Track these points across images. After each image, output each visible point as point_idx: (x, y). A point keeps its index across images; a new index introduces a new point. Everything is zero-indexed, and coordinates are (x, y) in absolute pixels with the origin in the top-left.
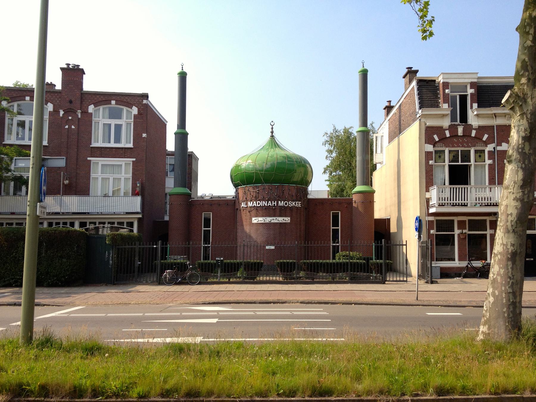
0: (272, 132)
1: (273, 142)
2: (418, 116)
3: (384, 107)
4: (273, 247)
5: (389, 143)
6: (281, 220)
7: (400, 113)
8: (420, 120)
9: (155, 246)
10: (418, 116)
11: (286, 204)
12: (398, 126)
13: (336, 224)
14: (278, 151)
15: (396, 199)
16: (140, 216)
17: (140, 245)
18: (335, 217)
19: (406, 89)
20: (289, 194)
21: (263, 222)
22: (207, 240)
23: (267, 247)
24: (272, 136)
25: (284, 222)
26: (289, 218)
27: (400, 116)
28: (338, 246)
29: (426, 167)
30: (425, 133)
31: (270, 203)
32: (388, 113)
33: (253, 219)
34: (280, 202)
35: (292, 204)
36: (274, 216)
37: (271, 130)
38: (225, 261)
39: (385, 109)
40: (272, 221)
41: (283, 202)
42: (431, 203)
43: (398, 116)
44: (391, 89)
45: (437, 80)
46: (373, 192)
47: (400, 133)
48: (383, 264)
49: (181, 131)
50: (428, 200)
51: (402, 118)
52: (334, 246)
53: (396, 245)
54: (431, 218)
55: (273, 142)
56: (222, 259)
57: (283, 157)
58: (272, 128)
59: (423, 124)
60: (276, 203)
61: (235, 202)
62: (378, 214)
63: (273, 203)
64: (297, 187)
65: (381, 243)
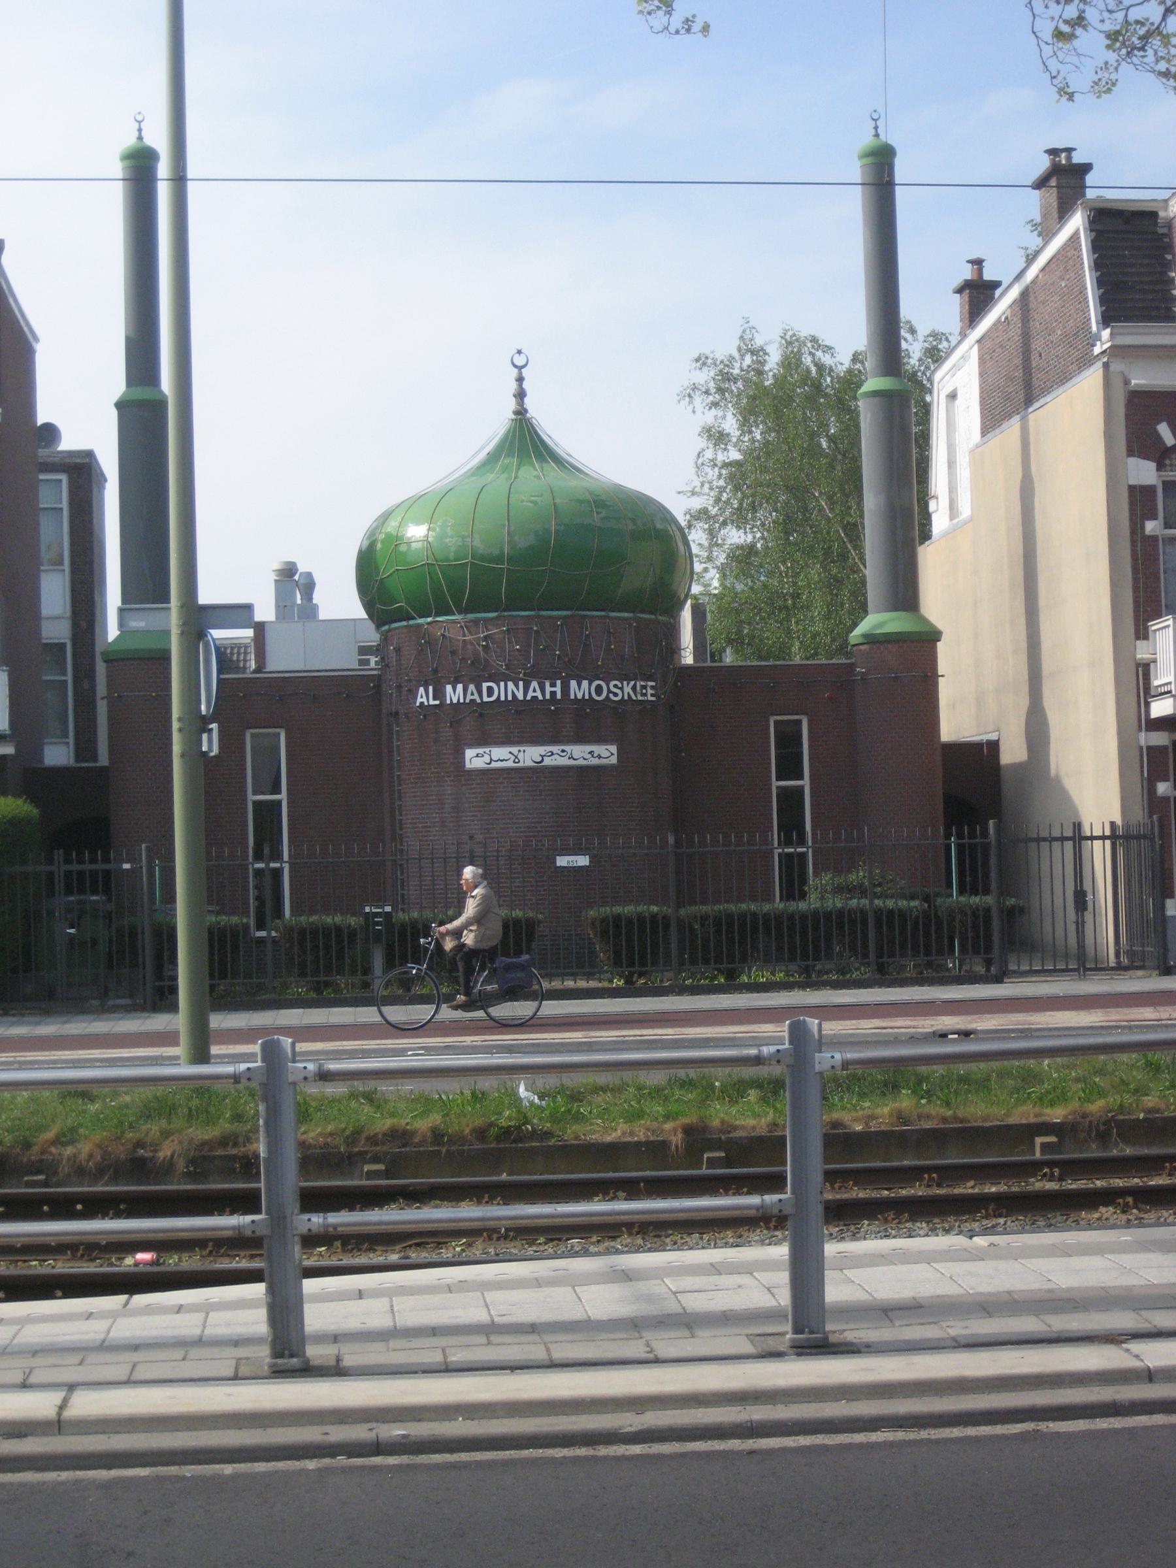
0: (521, 395)
1: (524, 441)
2: (1097, 350)
3: (958, 281)
4: (583, 861)
6: (580, 754)
8: (1106, 366)
9: (127, 866)
10: (1097, 350)
11: (599, 690)
12: (1019, 374)
13: (790, 766)
14: (552, 473)
18: (789, 739)
20: (608, 650)
21: (510, 764)
23: (562, 861)
24: (521, 412)
26: (613, 749)
27: (1026, 339)
28: (803, 856)
29: (1133, 542)
30: (1127, 416)
31: (534, 691)
33: (470, 753)
34: (573, 683)
35: (624, 690)
37: (514, 386)
38: (402, 916)
39: (959, 291)
40: (548, 761)
41: (585, 683)
42: (1156, 683)
43: (1015, 332)
44: (981, 224)
45: (1162, 214)
47: (1029, 400)
48: (995, 913)
49: (142, 393)
50: (1145, 670)
53: (1028, 840)
54: (1160, 739)
55: (524, 441)
56: (388, 909)
57: (580, 502)
58: (520, 380)
59: (1118, 383)
60: (558, 689)
61: (378, 688)
62: (955, 724)
63: (548, 689)
64: (638, 620)
65: (985, 833)
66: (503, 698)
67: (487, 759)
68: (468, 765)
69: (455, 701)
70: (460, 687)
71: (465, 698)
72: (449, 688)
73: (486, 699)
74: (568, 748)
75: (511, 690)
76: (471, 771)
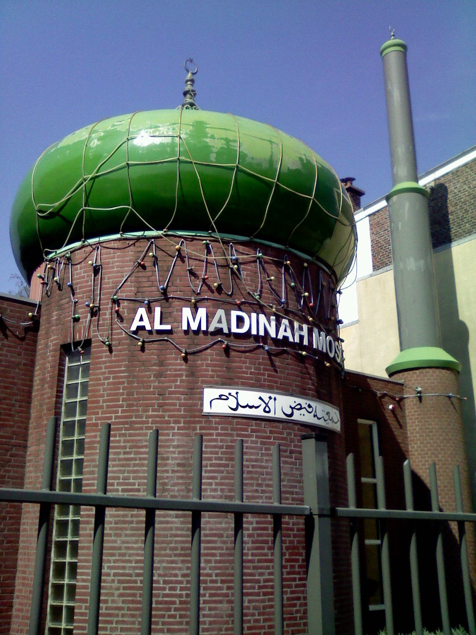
21: (259, 412)
33: (210, 393)
40: (297, 416)
66: (254, 332)
67: (232, 402)
68: (207, 409)
69: (194, 327)
70: (202, 312)
71: (277, 334)
72: (187, 312)
73: (234, 329)
74: (313, 404)
75: (257, 323)
76: (209, 416)
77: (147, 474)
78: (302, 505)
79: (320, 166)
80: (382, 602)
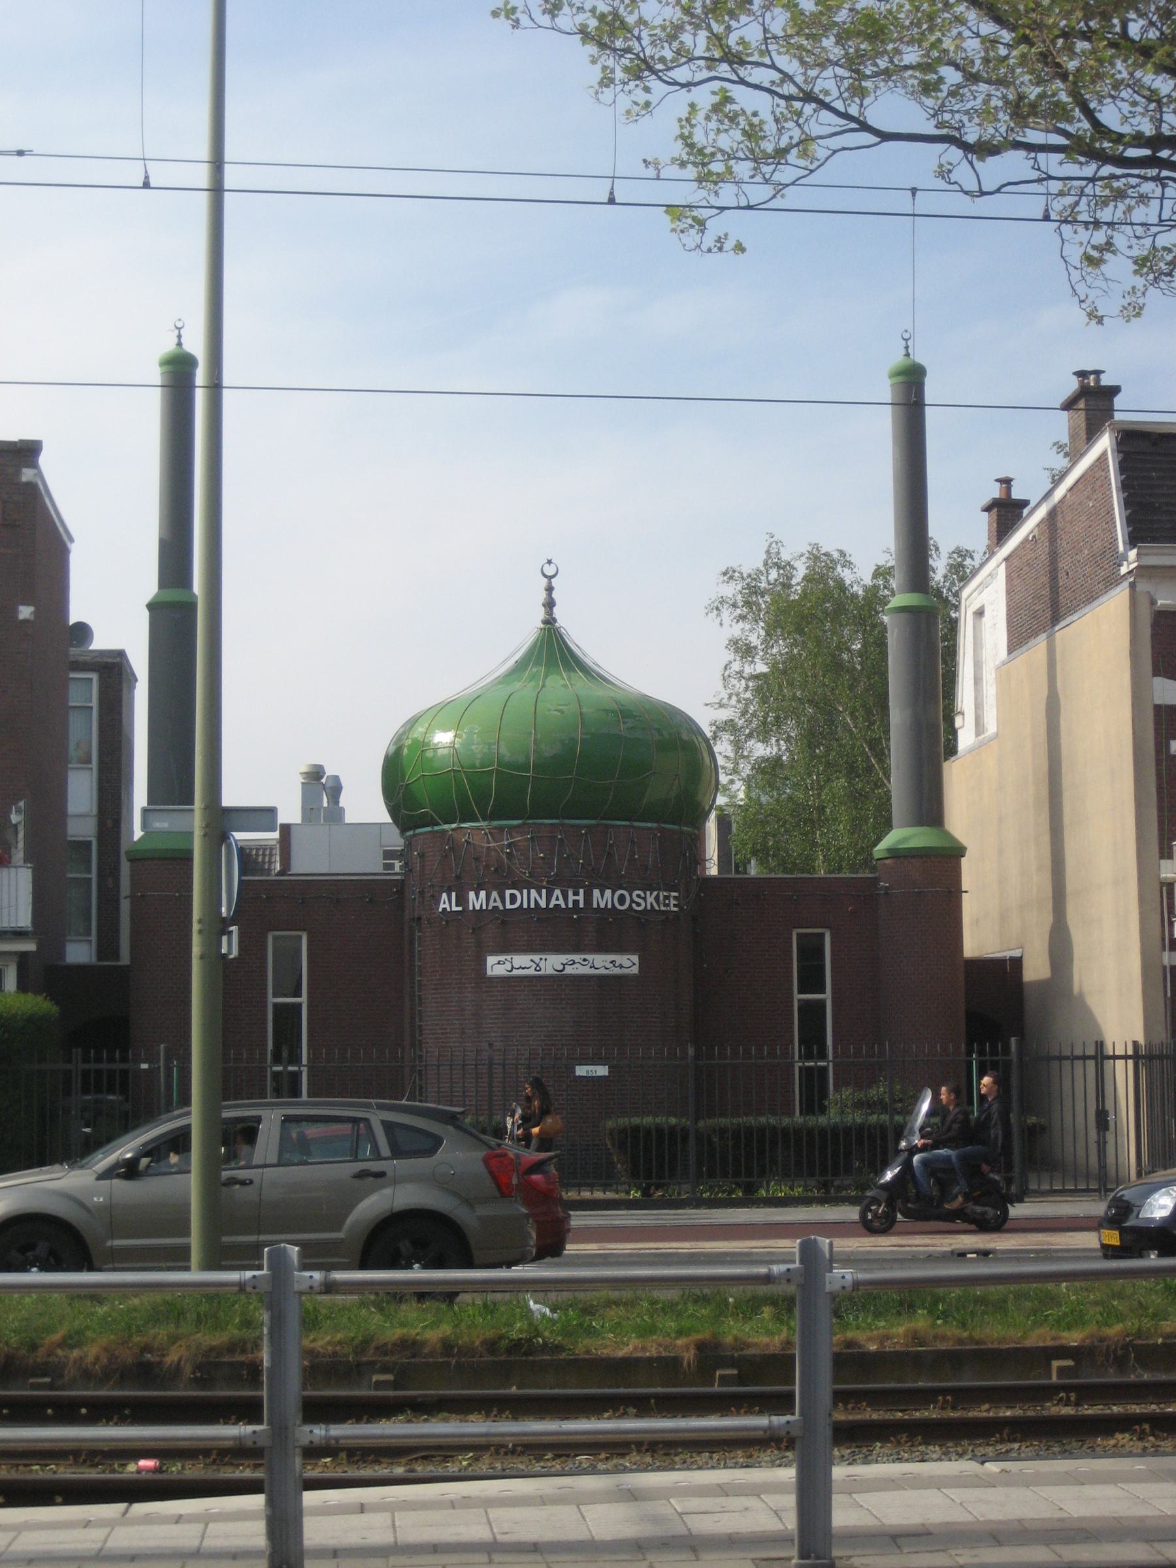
0: (550, 604)
1: (552, 650)
2: (1124, 570)
3: (986, 500)
4: (602, 1071)
5: (1011, 650)
6: (601, 963)
7: (1053, 540)
8: (1132, 586)
9: (144, 1066)
10: (1124, 570)
11: (622, 899)
12: (1046, 592)
15: (1042, 882)
16: (30, 946)
17: (86, 1060)
18: (811, 952)
19: (1075, 455)
21: (531, 972)
22: (813, 1040)
23: (581, 1071)
24: (550, 621)
25: (617, 971)
26: (635, 959)
28: (825, 1069)
29: (1158, 762)
31: (557, 899)
32: (1002, 531)
33: (491, 960)
34: (596, 893)
36: (577, 950)
37: (542, 596)
40: (569, 970)
41: (608, 892)
46: (956, 853)
47: (1056, 618)
49: (174, 595)
51: (1063, 564)
52: (807, 1073)
55: (552, 650)
60: (581, 898)
62: (979, 939)
63: (571, 898)
64: (662, 831)
65: (1007, 1050)
69: (478, 908)
70: (483, 894)
72: (472, 894)
73: (508, 906)
74: (590, 957)
75: (533, 898)
76: (491, 979)
77: (713, 870)
78: (180, 1269)
79: (1026, 511)
80: (823, 992)
